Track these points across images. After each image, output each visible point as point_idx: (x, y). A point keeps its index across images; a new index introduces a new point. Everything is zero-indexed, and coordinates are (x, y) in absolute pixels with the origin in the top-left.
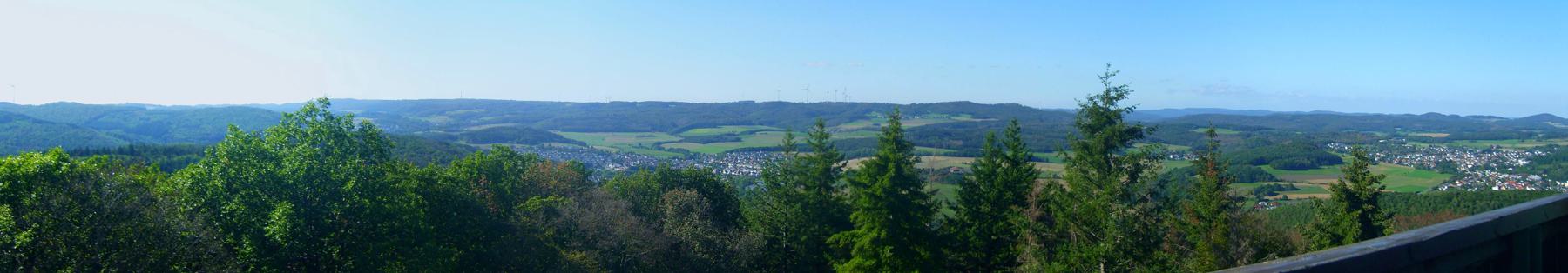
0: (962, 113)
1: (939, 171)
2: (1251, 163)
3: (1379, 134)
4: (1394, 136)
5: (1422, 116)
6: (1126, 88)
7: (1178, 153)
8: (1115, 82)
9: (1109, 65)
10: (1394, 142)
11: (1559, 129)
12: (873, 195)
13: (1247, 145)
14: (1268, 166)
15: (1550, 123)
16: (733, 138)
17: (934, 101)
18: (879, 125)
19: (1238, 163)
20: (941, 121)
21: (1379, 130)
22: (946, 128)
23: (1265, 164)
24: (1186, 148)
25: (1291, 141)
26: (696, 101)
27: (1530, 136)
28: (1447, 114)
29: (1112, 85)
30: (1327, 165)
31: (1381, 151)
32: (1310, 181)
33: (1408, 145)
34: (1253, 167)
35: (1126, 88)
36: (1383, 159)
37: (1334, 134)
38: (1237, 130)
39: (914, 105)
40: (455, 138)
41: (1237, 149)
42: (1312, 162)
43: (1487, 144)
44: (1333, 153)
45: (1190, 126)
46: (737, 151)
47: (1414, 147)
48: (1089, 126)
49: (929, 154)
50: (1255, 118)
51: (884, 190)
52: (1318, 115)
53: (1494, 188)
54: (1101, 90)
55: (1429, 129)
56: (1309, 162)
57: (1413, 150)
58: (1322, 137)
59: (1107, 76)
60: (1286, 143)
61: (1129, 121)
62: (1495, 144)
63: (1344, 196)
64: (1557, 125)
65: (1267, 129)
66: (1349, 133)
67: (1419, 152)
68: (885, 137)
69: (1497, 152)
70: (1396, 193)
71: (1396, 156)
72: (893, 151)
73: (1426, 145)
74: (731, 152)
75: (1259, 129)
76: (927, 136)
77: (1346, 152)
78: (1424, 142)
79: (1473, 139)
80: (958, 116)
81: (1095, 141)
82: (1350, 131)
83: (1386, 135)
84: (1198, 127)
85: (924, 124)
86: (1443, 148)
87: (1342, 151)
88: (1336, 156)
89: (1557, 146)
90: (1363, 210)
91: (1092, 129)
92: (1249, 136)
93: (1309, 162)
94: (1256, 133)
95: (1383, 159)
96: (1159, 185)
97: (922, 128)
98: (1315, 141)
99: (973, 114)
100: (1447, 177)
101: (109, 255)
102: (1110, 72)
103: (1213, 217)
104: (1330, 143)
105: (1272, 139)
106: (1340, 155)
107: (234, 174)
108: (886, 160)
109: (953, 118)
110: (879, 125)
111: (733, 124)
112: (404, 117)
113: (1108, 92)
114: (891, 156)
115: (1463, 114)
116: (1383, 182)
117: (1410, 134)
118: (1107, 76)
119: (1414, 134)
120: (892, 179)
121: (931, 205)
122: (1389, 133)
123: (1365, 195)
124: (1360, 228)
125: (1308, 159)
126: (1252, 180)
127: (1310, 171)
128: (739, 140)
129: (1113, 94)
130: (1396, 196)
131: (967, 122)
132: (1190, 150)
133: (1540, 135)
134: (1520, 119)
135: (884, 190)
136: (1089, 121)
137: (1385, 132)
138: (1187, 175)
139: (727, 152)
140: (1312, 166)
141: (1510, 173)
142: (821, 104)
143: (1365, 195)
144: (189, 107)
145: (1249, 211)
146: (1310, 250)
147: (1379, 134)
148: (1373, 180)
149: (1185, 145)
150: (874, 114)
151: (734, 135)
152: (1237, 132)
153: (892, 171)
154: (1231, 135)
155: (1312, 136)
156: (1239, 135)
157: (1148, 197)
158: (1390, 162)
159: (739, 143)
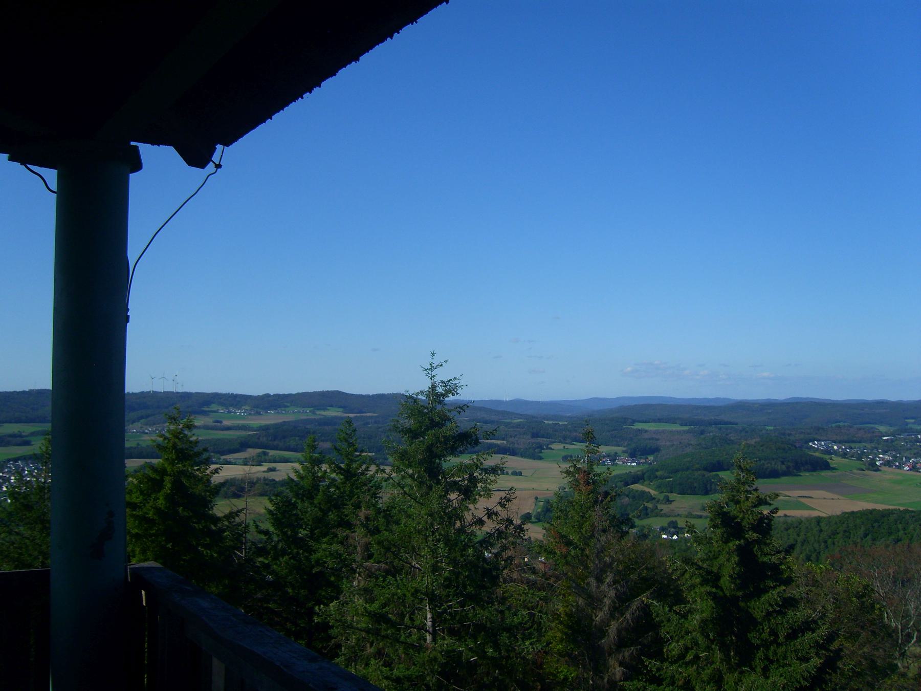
0: (332, 406)
2: (705, 469)
3: (882, 428)
4: (905, 431)
6: (457, 381)
7: (608, 456)
8: (442, 375)
9: (433, 354)
10: (905, 439)
12: (144, 519)
13: (699, 445)
14: (728, 473)
16: (19, 440)
17: (294, 391)
18: (221, 422)
19: (688, 469)
20: (304, 417)
21: (881, 423)
22: (308, 427)
23: (725, 470)
24: (619, 449)
25: (758, 440)
26: (27, 389)
29: (438, 379)
30: (808, 470)
31: (884, 453)
32: (787, 493)
34: (707, 474)
35: (457, 381)
36: (888, 463)
37: (818, 429)
38: (686, 425)
39: (268, 395)
41: (689, 450)
42: (788, 467)
44: (817, 454)
45: (625, 420)
46: (24, 458)
48: (409, 431)
49: (286, 461)
51: (158, 511)
52: (797, 403)
54: (426, 385)
56: (784, 467)
58: (801, 433)
59: (432, 368)
60: (752, 442)
61: (463, 423)
63: (719, 521)
65: (726, 423)
66: (839, 427)
68: (268, 431)
70: (906, 511)
71: (908, 459)
72: (172, 463)
74: (16, 460)
75: (716, 423)
76: (284, 437)
77: (836, 453)
80: (325, 409)
81: (417, 448)
82: (841, 424)
83: (892, 429)
84: (634, 422)
85: (281, 421)
87: (829, 452)
88: (821, 459)
90: (746, 539)
91: (414, 434)
92: (702, 433)
93: (784, 467)
94: (713, 428)
95: (888, 463)
96: (500, 503)
97: (276, 426)
98: (792, 438)
99: (346, 408)
101: (772, 512)
102: (436, 362)
103: (585, 544)
104: (813, 441)
105: (733, 437)
106: (826, 457)
108: (162, 472)
109: (318, 412)
110: (221, 422)
111: (18, 421)
113: (433, 387)
114: (169, 469)
116: (775, 504)
118: (432, 368)
120: (167, 497)
122: (896, 428)
123: (748, 520)
124: (737, 564)
125: (783, 463)
126: (706, 492)
127: (784, 479)
128: (27, 443)
129: (440, 390)
130: (907, 516)
131: (336, 417)
132: (624, 452)
135: (158, 511)
136: (409, 423)
137: (891, 425)
138: (619, 484)
139: (9, 460)
140: (786, 473)
143: (748, 520)
147: (882, 428)
148: (761, 502)
149: (619, 446)
150: (214, 407)
151: (20, 436)
152: (686, 428)
153: (168, 485)
154: (678, 432)
155: (788, 432)
156: (688, 432)
157: (485, 519)
158: (899, 467)
159: (28, 448)
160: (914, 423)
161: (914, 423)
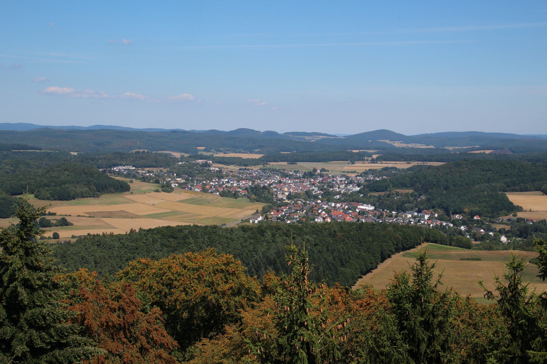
1: (117, 236)
3: (177, 155)
11: (399, 149)
15: (388, 141)
27: (360, 158)
33: (215, 168)
36: (181, 185)
40: (248, 221)
43: (309, 166)
47: (220, 171)
53: (319, 220)
57: (220, 175)
62: (319, 166)
67: (227, 176)
78: (233, 164)
79: (293, 161)
100: (260, 206)
112: (17, 144)
117: (215, 155)
119: (221, 155)
121: (88, 325)
133: (375, 157)
134: (351, 136)
141: (336, 201)
145: (228, 290)
160: (204, 150)
161: (204, 150)
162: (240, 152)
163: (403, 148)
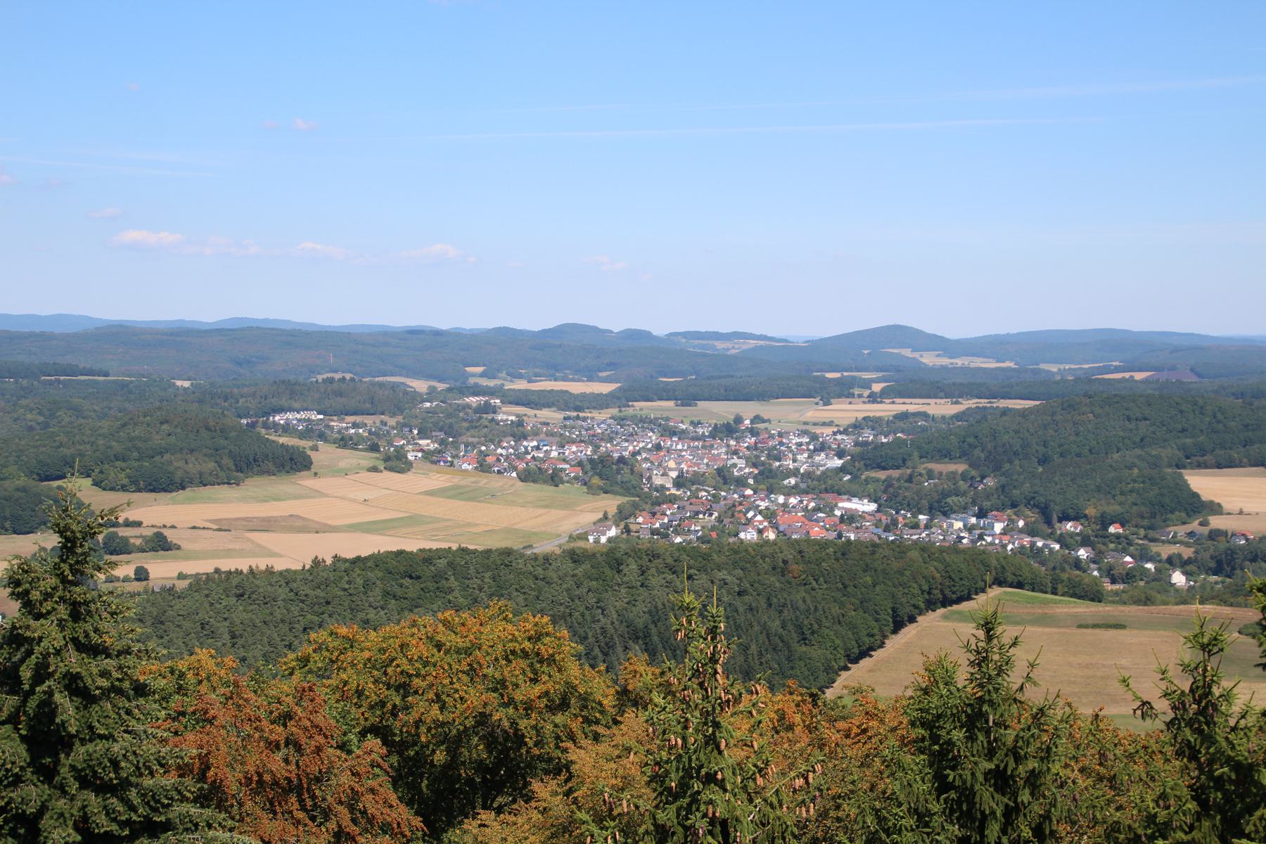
3: (420, 386)
5: (545, 332)
11: (933, 369)
27: (844, 390)
28: (655, 334)
33: (507, 415)
43: (724, 410)
50: (44, 338)
53: (748, 535)
55: (554, 371)
57: (518, 431)
62: (747, 410)
64: (929, 359)
69: (753, 432)
73: (552, 415)
79: (688, 398)
86: (601, 419)
89: (924, 415)
107: (480, 766)
112: (52, 362)
115: (660, 329)
117: (508, 386)
119: (521, 385)
133: (877, 388)
141: (789, 492)
142: (1019, 334)
144: (595, 329)
146: (1098, 774)
147: (420, 386)
160: (482, 375)
161: (482, 375)
162: (565, 379)
163: (943, 368)
